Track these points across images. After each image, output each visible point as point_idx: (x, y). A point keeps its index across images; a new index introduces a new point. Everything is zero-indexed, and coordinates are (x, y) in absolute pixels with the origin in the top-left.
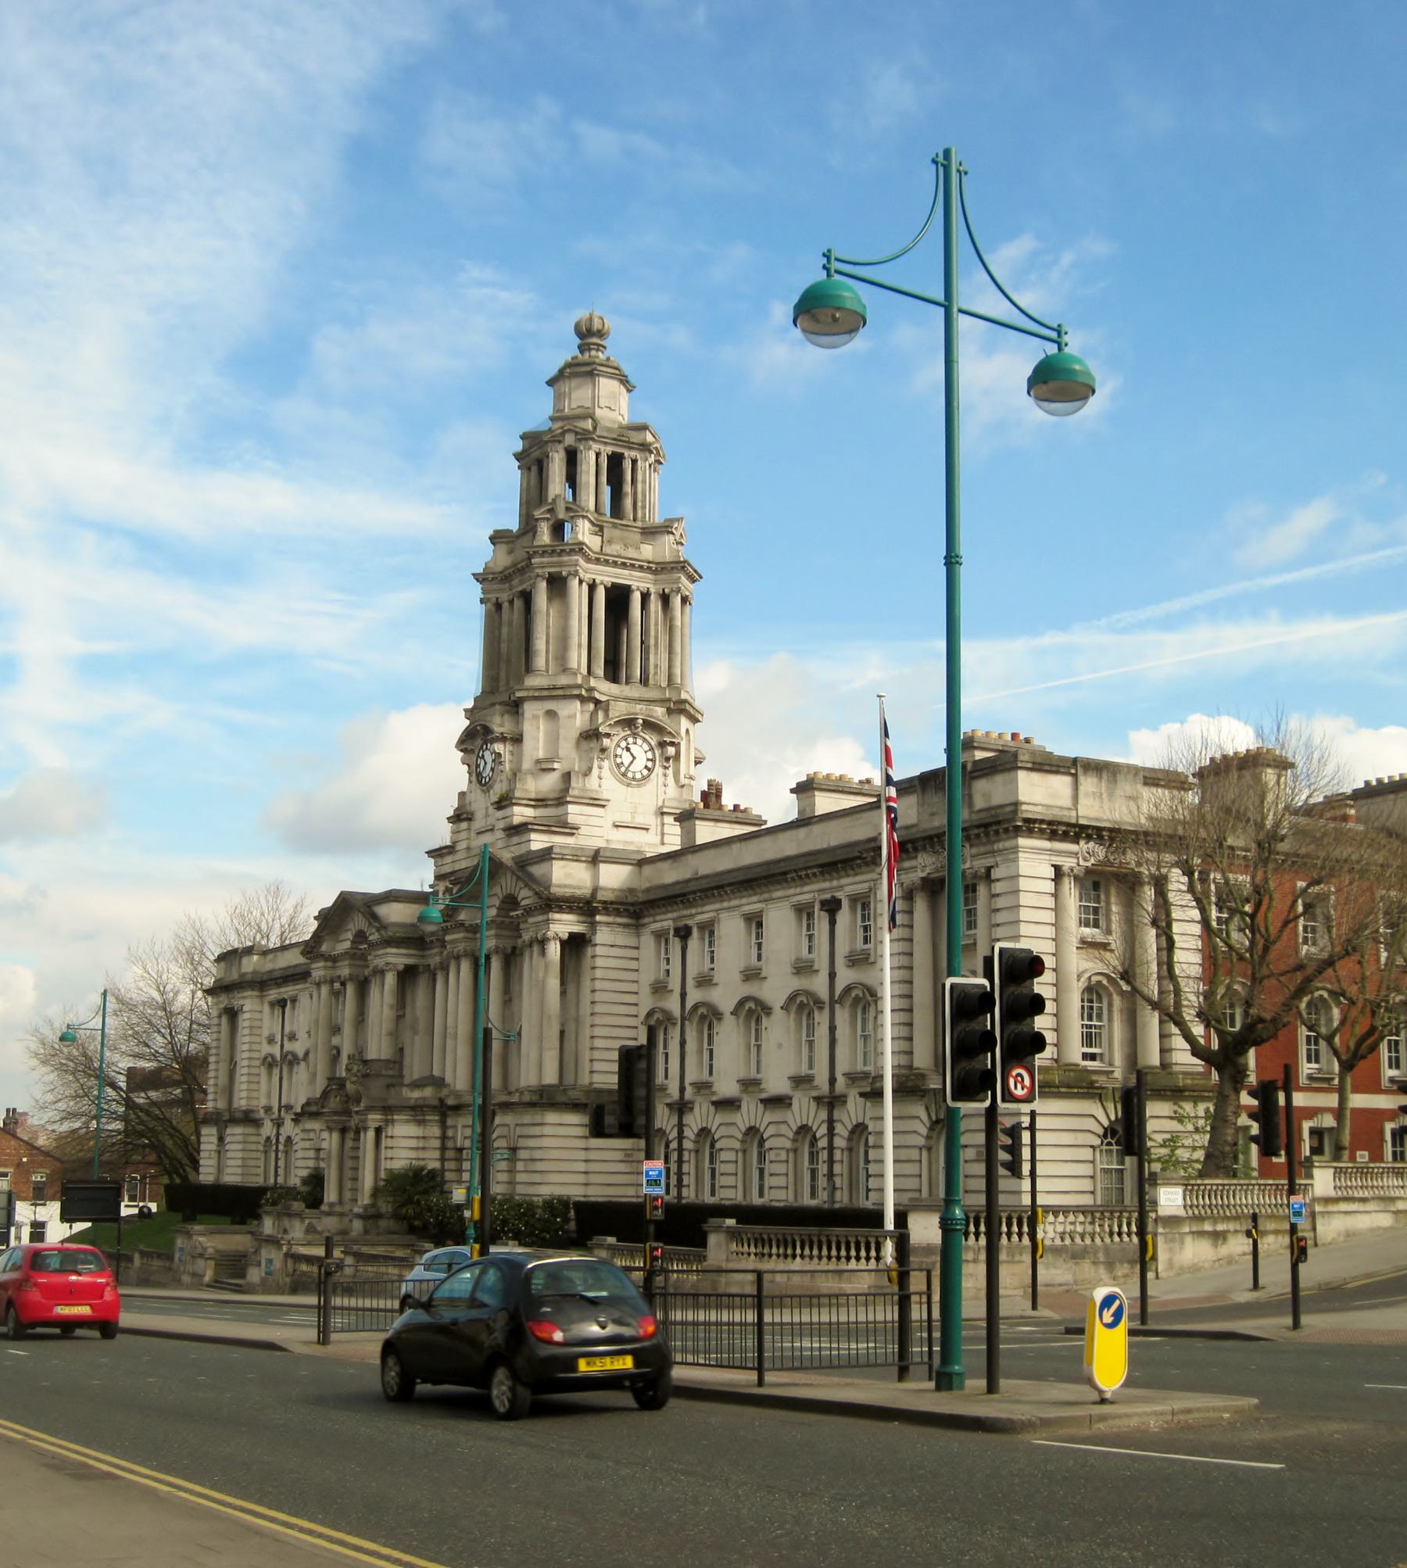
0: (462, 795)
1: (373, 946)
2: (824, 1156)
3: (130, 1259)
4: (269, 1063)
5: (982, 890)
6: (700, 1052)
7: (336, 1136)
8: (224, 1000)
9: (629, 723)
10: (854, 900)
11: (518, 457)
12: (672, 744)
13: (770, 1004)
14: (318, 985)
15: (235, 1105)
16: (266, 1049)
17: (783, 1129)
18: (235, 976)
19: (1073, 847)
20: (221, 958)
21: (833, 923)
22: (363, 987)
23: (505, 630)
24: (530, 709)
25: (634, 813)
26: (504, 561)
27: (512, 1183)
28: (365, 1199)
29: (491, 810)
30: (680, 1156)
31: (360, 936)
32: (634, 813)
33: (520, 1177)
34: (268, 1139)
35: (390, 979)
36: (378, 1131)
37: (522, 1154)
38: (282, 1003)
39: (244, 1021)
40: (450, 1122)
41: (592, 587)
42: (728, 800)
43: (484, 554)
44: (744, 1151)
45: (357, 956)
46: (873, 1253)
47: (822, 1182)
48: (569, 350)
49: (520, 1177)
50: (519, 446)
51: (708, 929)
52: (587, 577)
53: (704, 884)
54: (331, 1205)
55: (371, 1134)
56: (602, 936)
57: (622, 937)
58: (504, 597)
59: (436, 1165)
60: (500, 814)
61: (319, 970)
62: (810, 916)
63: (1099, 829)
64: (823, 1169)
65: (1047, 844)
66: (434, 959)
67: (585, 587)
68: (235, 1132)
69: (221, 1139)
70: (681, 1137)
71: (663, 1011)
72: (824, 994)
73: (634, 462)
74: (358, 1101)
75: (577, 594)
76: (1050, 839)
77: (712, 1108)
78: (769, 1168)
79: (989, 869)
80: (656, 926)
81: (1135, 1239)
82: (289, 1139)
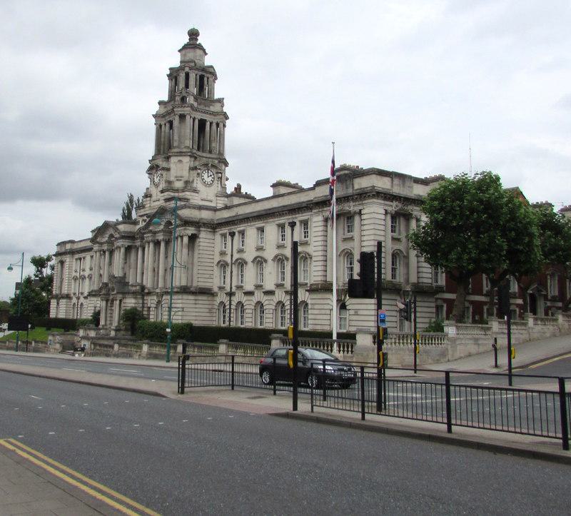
0: (148, 189)
1: (117, 239)
2: (228, 311)
3: (31, 343)
4: (75, 279)
5: (357, 218)
6: (238, 275)
7: (104, 302)
8: (59, 258)
9: (206, 165)
10: (239, 232)
11: (168, 76)
12: (221, 173)
13: (247, 260)
14: (96, 252)
15: (63, 292)
16: (74, 274)
17: (272, 302)
18: (63, 250)
19: (391, 203)
20: (58, 245)
21: (293, 230)
22: (111, 253)
23: (163, 134)
26: (163, 111)
27: (170, 319)
28: (115, 324)
29: (159, 194)
30: (230, 311)
31: (111, 236)
34: (74, 304)
35: (123, 250)
36: (121, 301)
39: (66, 265)
40: (145, 298)
41: (194, 119)
42: (243, 191)
43: (156, 108)
44: (276, 310)
45: (110, 242)
46: (350, 349)
47: (227, 319)
48: (186, 39)
51: (242, 233)
52: (193, 116)
53: (241, 217)
54: (103, 326)
55: (118, 302)
57: (210, 236)
58: (163, 123)
59: (141, 309)
60: (162, 194)
61: (96, 247)
62: (225, 237)
63: (400, 197)
64: (227, 315)
65: (383, 202)
66: (138, 243)
68: (63, 302)
69: (58, 304)
70: (230, 304)
71: (224, 261)
72: (229, 261)
73: (208, 78)
74: (113, 291)
75: (189, 121)
76: (383, 200)
77: (243, 295)
78: (265, 316)
79: (360, 210)
80: (221, 232)
81: (413, 345)
82: (82, 304)
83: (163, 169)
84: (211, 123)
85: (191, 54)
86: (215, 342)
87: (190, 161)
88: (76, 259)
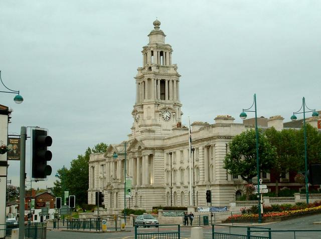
16: (165, 167)
22: (141, 158)
24: (145, 107)
25: (167, 127)
32: (167, 127)
33: (142, 202)
35: (147, 157)
37: (142, 197)
38: (103, 165)
41: (157, 81)
43: (136, 73)
48: (152, 28)
49: (142, 202)
50: (142, 49)
55: (115, 194)
56: (156, 154)
58: (140, 82)
65: (224, 140)
67: (156, 81)
83: (140, 112)
84: (169, 81)
85: (157, 39)
86: (43, 178)
87: (155, 107)
88: (167, 154)
